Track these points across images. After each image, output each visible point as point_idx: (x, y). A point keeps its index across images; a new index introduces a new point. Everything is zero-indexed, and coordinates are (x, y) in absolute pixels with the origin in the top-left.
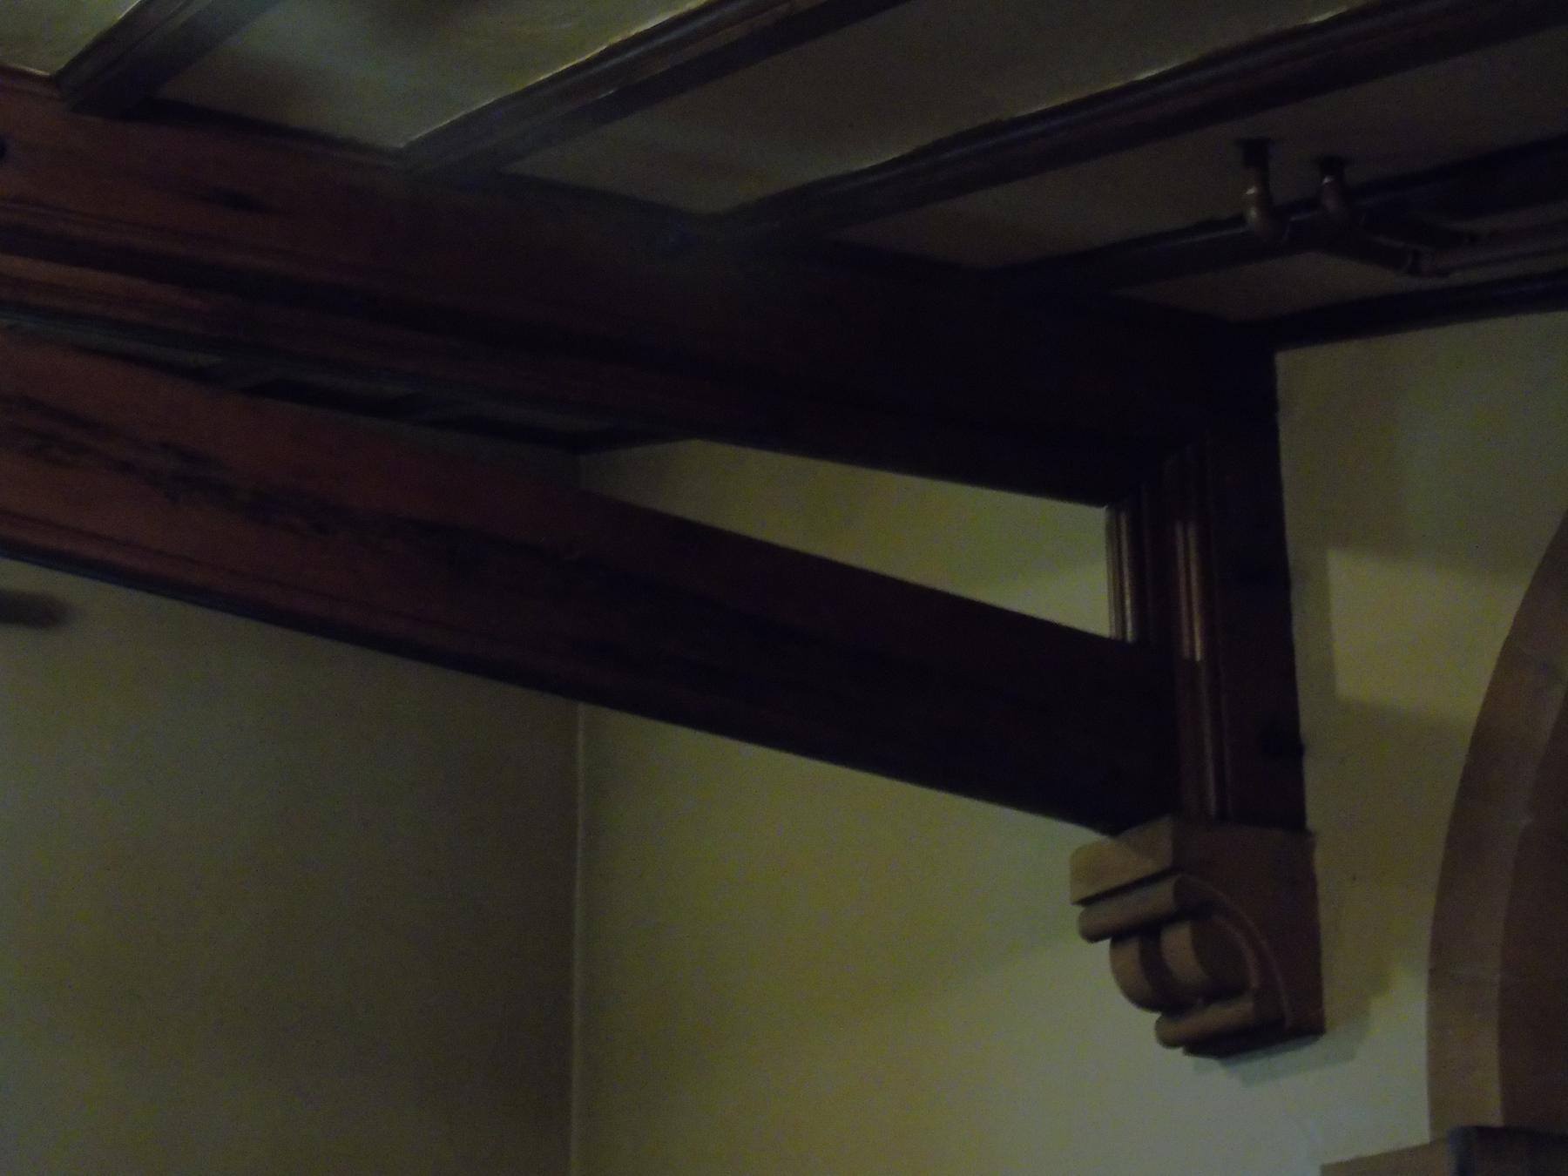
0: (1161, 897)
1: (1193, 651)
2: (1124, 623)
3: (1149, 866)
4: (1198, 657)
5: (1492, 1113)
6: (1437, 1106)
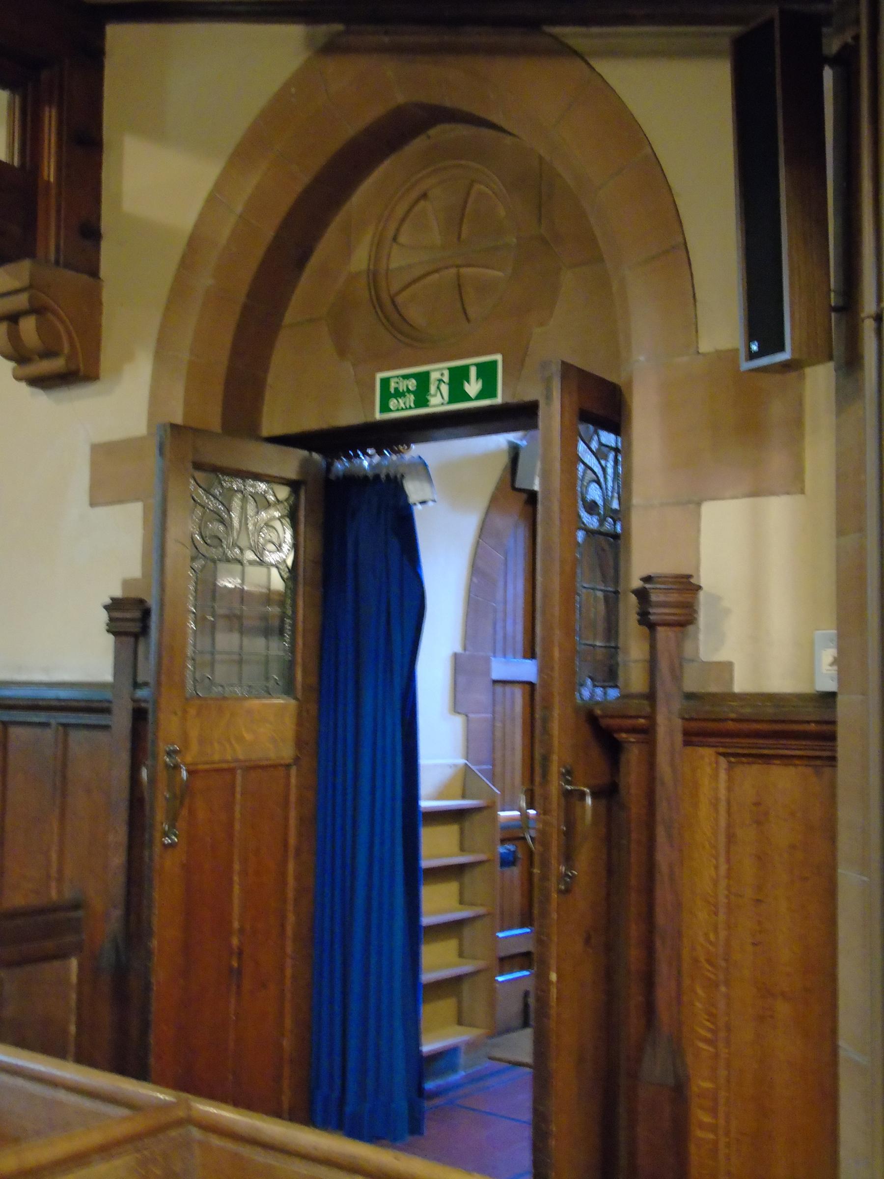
0: (21, 301)
1: (49, 176)
2: (13, 155)
3: (16, 284)
4: (52, 180)
5: (179, 420)
6: (151, 415)
